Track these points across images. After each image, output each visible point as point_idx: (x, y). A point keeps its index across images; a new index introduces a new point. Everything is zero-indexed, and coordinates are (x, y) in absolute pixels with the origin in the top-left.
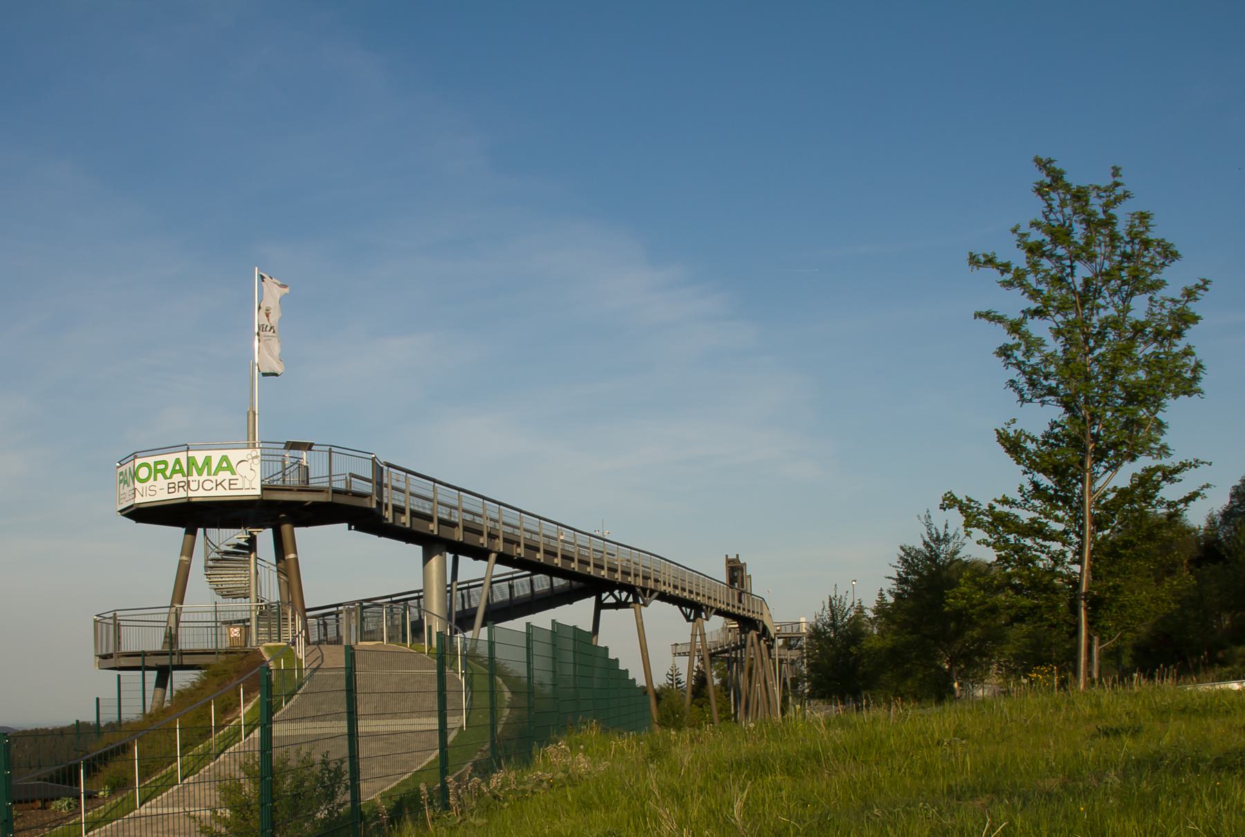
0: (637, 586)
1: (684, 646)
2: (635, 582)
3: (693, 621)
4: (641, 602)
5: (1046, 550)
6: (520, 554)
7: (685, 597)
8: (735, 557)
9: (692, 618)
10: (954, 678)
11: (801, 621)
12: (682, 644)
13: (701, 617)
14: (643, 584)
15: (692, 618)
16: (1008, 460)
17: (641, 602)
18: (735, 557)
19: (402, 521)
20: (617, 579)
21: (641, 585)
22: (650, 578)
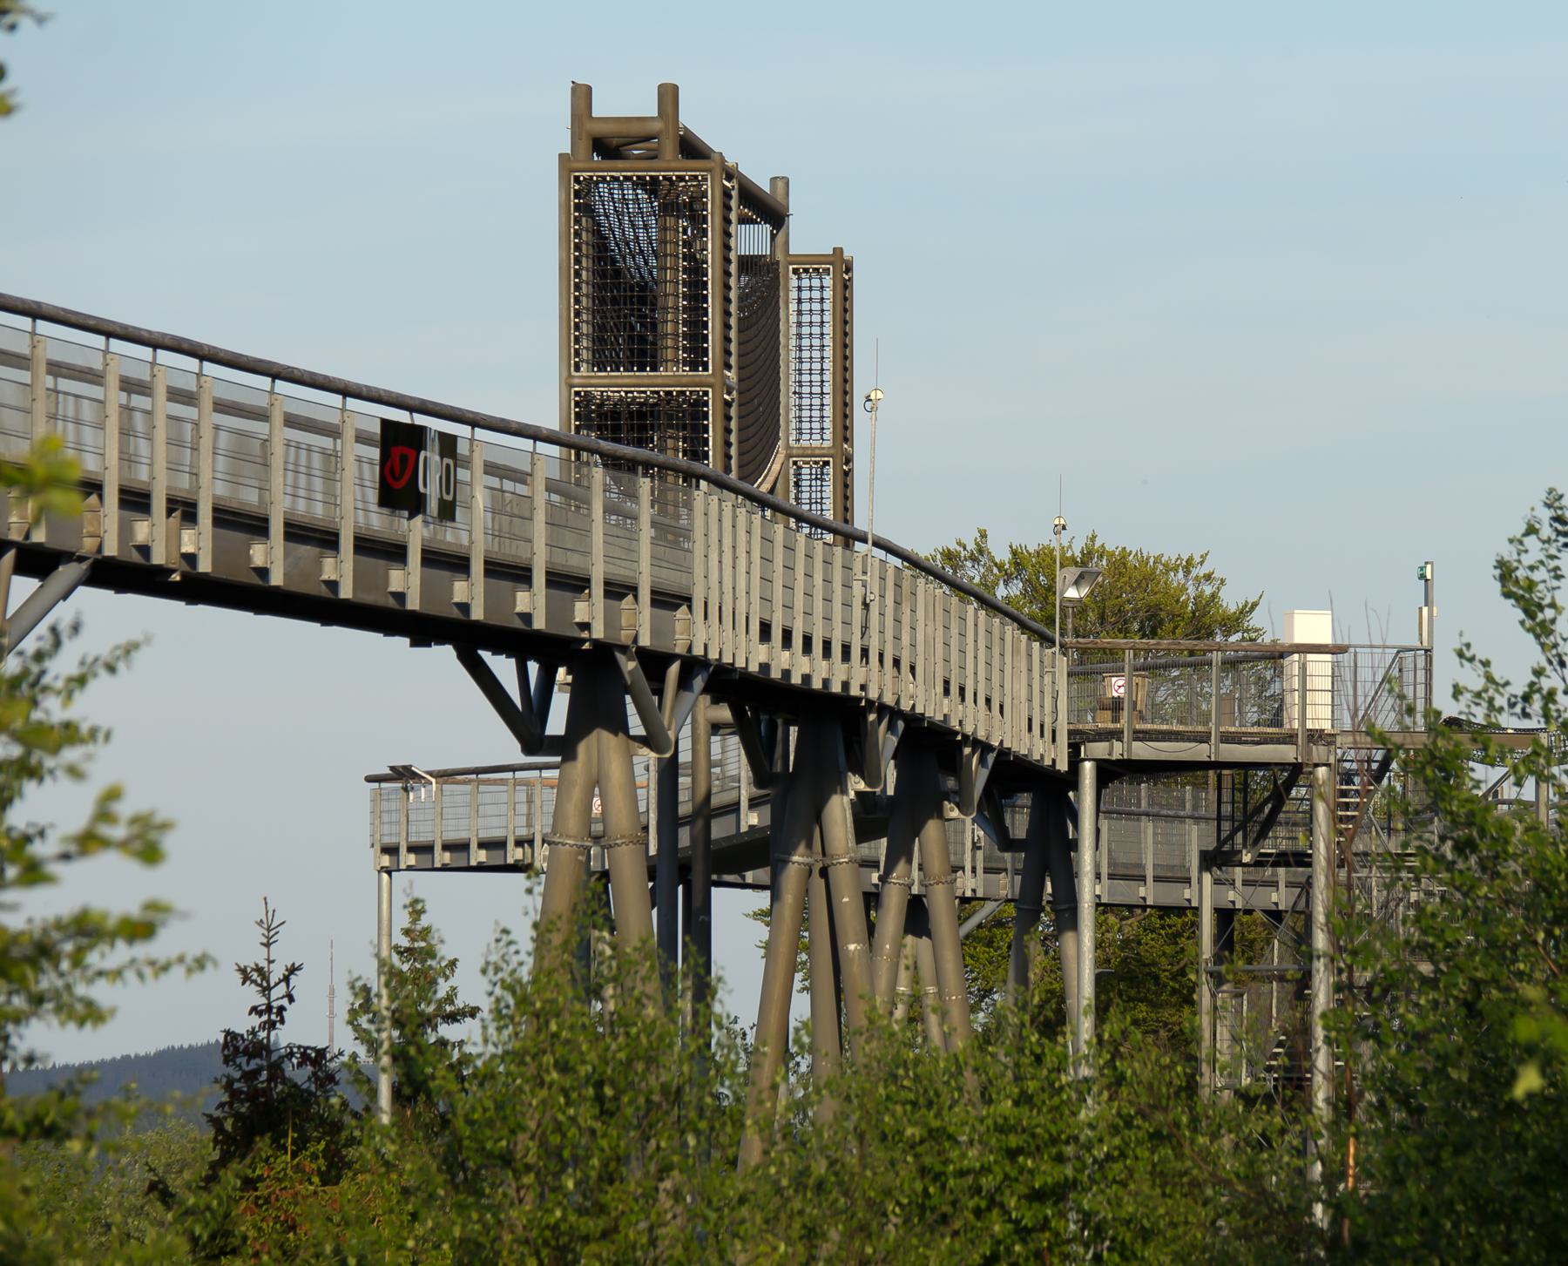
0: (624, 649)
1: (457, 792)
2: (611, 621)
3: (565, 747)
4: (636, 726)
5: (273, 1017)
6: (191, 559)
7: (527, 618)
8: (648, 107)
9: (556, 724)
10: (574, 961)
11: (1300, 638)
12: (445, 776)
13: (618, 725)
14: (654, 633)
15: (556, 724)
16: (122, 639)
17: (636, 726)
18: (648, 107)
19: (392, 588)
20: (585, 626)
21: (645, 641)
22: (634, 590)
